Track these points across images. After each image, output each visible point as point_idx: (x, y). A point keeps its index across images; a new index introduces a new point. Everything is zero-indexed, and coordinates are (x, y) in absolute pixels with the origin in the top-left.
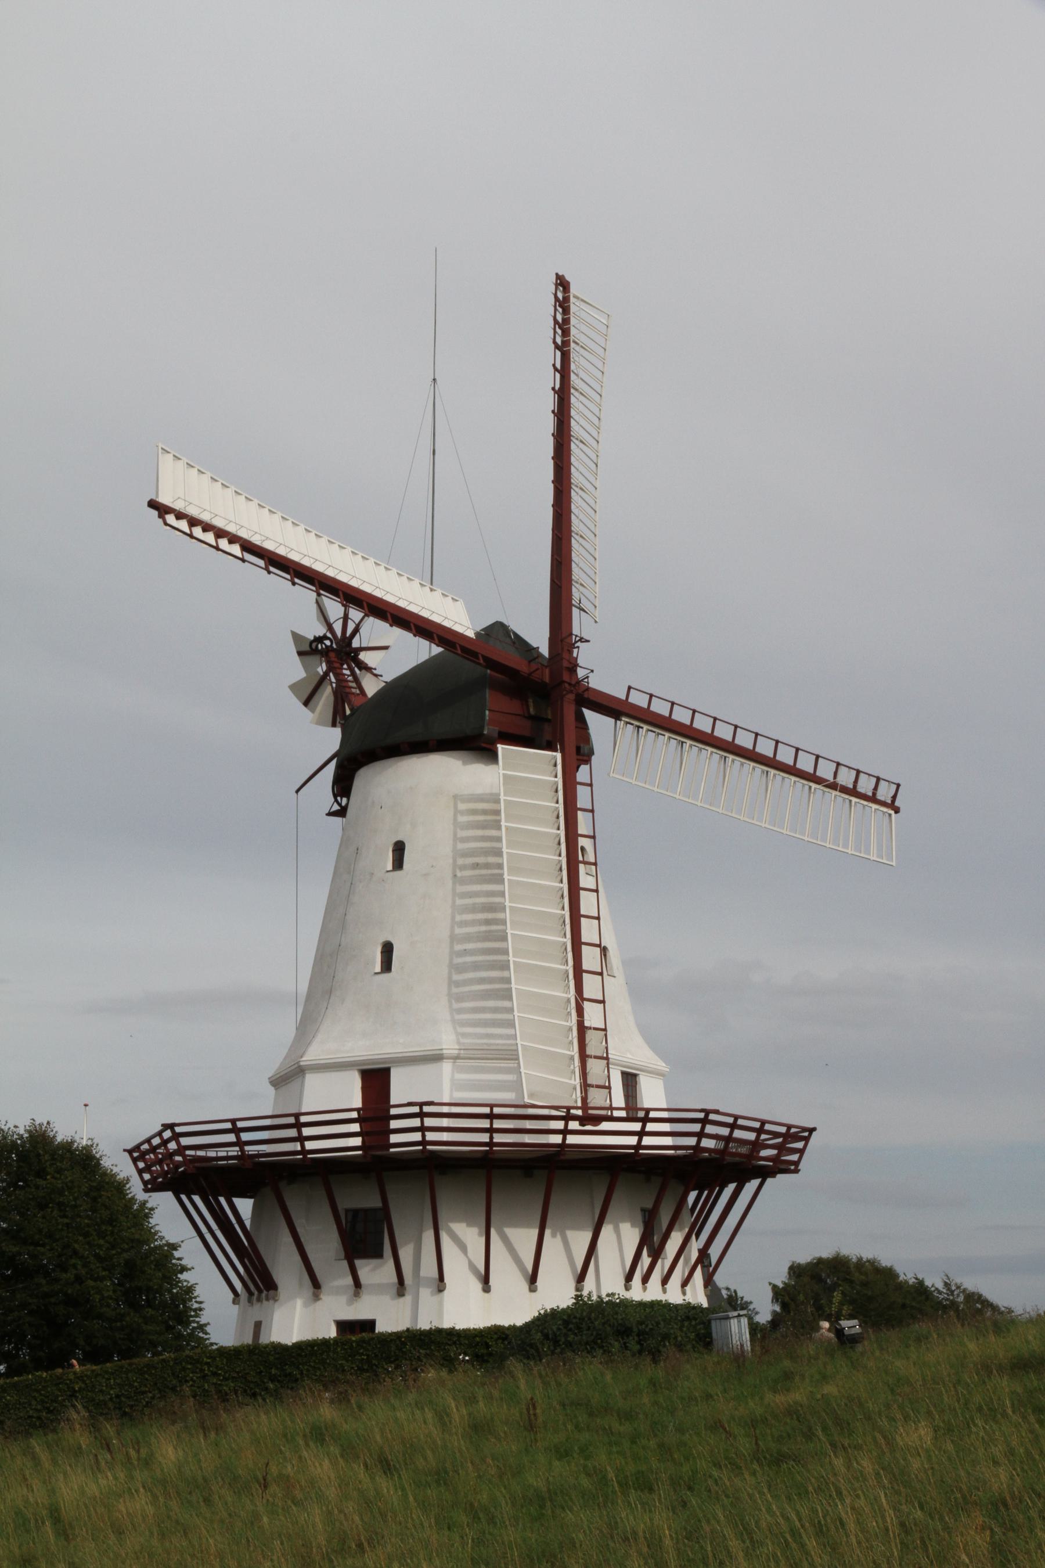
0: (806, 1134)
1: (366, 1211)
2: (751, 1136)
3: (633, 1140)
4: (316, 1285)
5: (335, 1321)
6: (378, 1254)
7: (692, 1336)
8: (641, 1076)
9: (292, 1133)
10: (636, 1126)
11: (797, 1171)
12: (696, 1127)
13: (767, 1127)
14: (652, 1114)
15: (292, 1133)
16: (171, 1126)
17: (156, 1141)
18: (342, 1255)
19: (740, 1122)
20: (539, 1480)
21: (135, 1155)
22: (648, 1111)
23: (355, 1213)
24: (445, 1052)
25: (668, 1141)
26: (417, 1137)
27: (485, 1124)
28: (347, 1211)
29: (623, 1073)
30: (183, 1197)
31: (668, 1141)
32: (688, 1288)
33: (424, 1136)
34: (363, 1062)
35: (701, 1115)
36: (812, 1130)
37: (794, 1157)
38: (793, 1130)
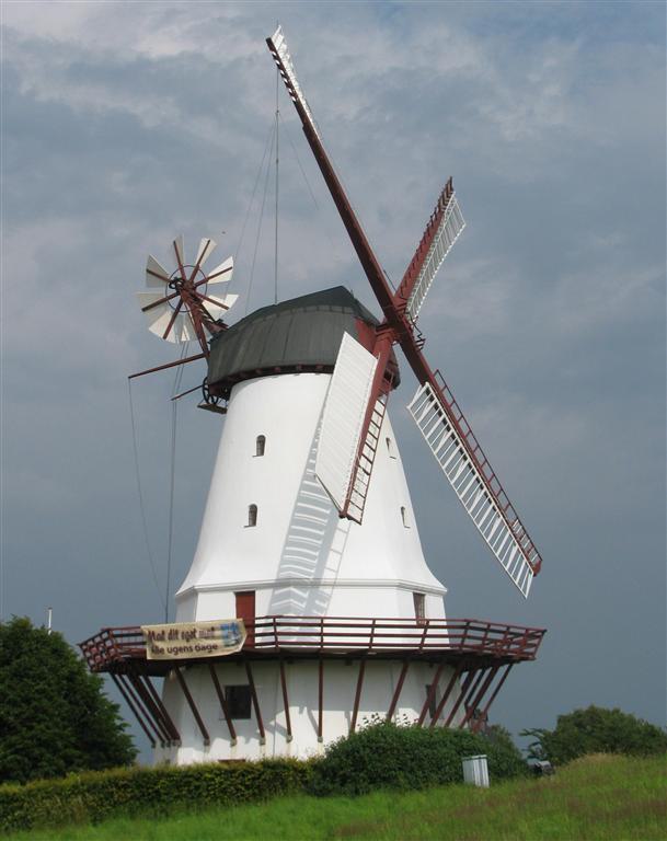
0: (539, 634)
1: (240, 687)
2: (500, 637)
3: (418, 641)
6: (247, 715)
8: (426, 598)
10: (421, 631)
11: (533, 659)
12: (461, 632)
13: (512, 630)
14: (431, 623)
16: (108, 631)
17: (98, 640)
18: (223, 717)
19: (492, 627)
21: (84, 647)
22: (428, 621)
23: (232, 690)
25: (446, 641)
27: (368, 631)
28: (227, 688)
29: (415, 594)
30: (117, 676)
31: (446, 641)
33: (276, 638)
34: (237, 588)
35: (465, 624)
36: (544, 632)
37: (532, 650)
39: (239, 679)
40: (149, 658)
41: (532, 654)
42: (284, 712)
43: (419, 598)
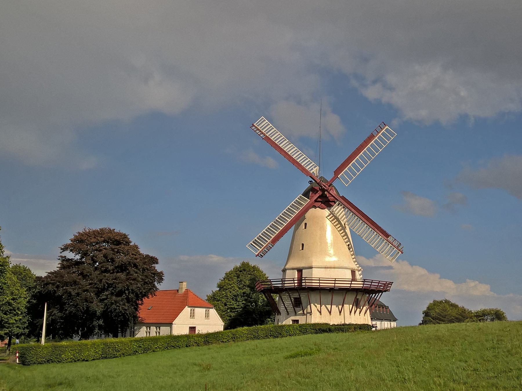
0: (391, 283)
3: (349, 285)
4: (296, 313)
5: (292, 320)
7: (485, 339)
9: (293, 282)
11: (389, 291)
15: (293, 282)
20: (5, 272)
23: (295, 299)
24: (313, 266)
26: (333, 285)
27: (334, 282)
32: (366, 315)
37: (389, 288)
38: (387, 283)
39: (296, 295)
40: (319, 199)
41: (389, 289)
42: (309, 305)
43: (353, 272)
